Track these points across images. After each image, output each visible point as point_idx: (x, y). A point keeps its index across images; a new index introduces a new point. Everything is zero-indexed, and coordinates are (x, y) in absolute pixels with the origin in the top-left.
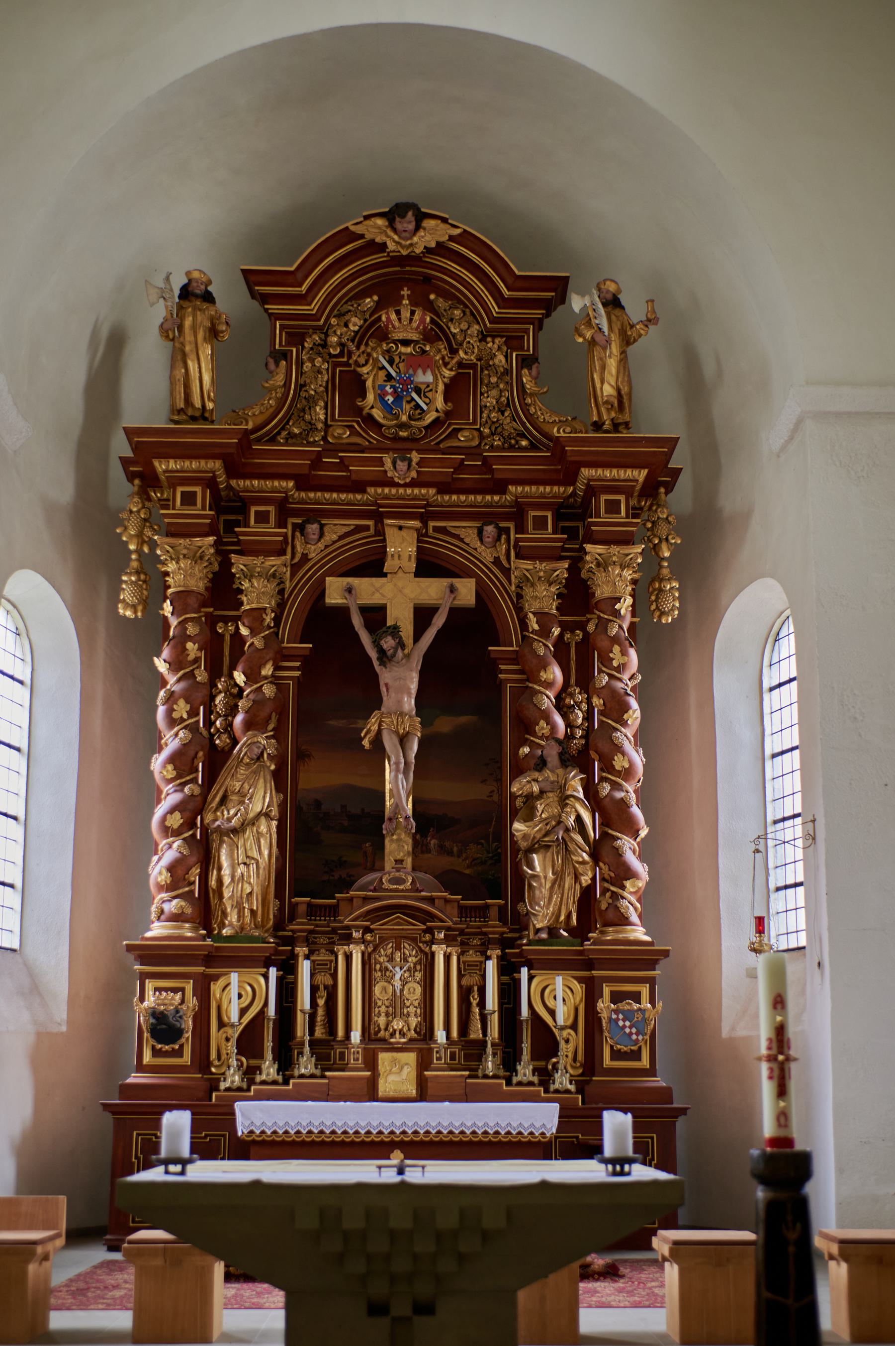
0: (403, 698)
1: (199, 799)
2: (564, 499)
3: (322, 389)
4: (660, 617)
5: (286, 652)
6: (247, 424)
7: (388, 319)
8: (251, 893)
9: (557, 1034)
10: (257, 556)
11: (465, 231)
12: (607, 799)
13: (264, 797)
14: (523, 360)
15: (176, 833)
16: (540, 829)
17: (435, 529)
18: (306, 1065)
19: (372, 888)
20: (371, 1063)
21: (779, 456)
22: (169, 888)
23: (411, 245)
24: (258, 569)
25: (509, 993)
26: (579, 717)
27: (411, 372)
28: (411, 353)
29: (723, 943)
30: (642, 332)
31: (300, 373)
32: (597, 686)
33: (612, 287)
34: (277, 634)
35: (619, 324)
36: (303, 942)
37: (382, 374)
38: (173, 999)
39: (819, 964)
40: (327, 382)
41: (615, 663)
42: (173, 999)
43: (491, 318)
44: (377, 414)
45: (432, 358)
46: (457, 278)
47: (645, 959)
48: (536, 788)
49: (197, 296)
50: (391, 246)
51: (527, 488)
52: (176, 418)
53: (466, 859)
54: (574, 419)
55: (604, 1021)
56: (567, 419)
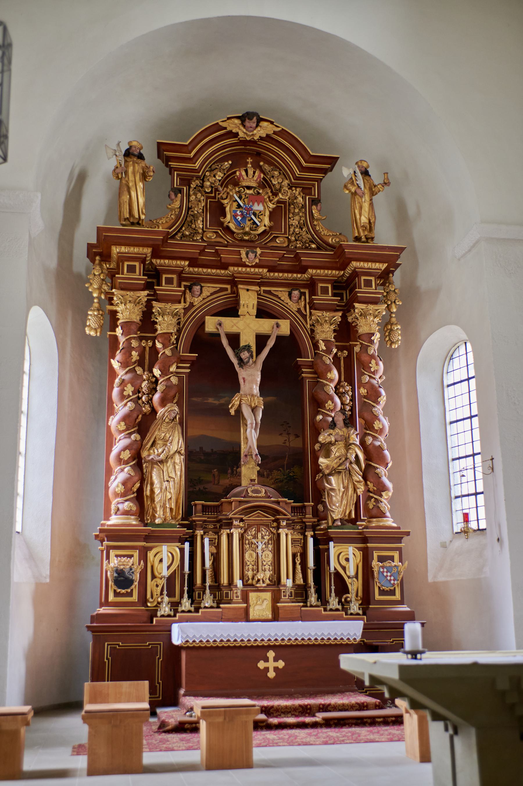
0: (253, 387)
1: (139, 442)
2: (338, 278)
3: (201, 211)
4: (391, 345)
6: (158, 228)
7: (241, 174)
8: (171, 498)
9: (347, 581)
10: (167, 303)
12: (371, 446)
13: (178, 442)
14: (313, 201)
15: (126, 463)
16: (337, 463)
17: (265, 291)
18: (208, 601)
19: (243, 495)
20: (245, 599)
21: (459, 260)
22: (123, 495)
23: (253, 135)
24: (168, 311)
25: (321, 557)
27: (251, 204)
28: (252, 194)
29: (427, 528)
30: (381, 189)
31: (189, 201)
32: (363, 382)
33: (365, 164)
34: (177, 347)
36: (200, 527)
37: (235, 204)
38: (129, 561)
39: (498, 539)
41: (372, 370)
42: (129, 561)
43: (295, 177)
44: (232, 226)
45: (263, 197)
47: (395, 537)
48: (333, 439)
49: (134, 155)
50: (241, 134)
51: (319, 271)
53: (272, 479)
54: (340, 234)
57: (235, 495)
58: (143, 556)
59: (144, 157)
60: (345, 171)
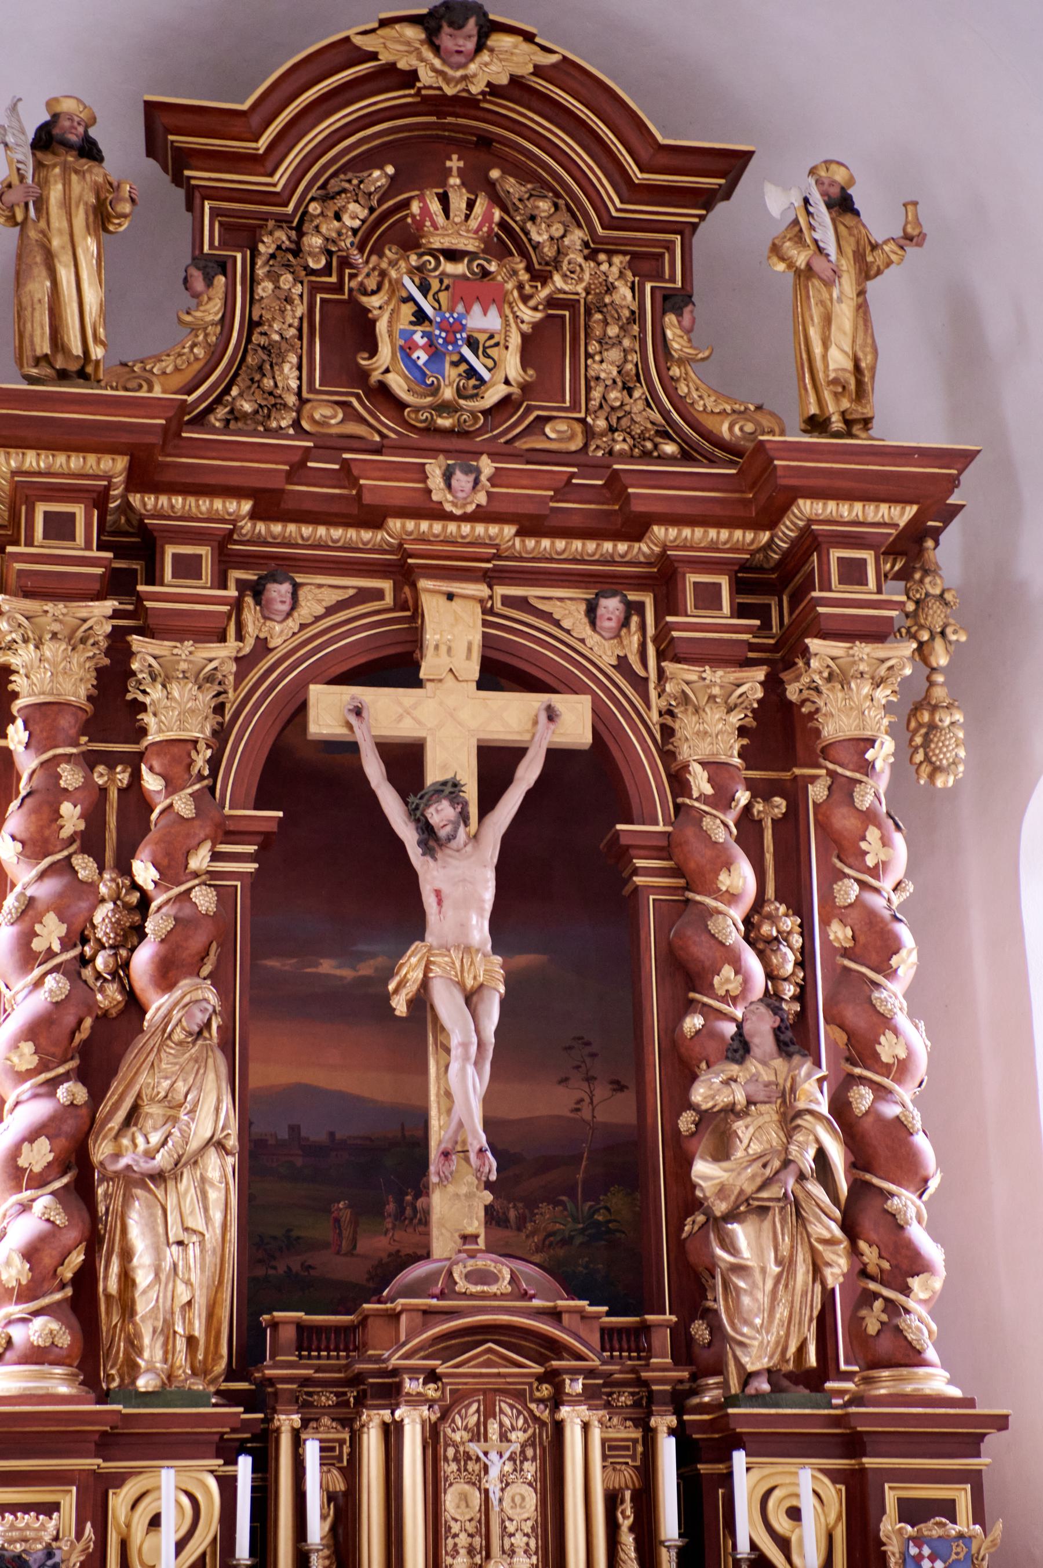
0: (469, 919)
1: (84, 1111)
2: (753, 553)
3: (293, 331)
4: (931, 777)
5: (231, 826)
6: (150, 390)
8: (189, 1303)
10: (182, 641)
11: (565, 58)
12: (870, 1119)
13: (217, 1110)
14: (666, 298)
15: (39, 1181)
16: (753, 1177)
17: (507, 601)
19: (437, 1290)
23: (465, 78)
24: (183, 666)
26: (787, 960)
27: (460, 308)
28: (464, 276)
30: (893, 257)
31: (252, 299)
33: (840, 175)
34: (212, 789)
35: (852, 240)
36: (289, 1403)
37: (407, 310)
38: (43, 1527)
40: (301, 319)
41: (870, 861)
44: (397, 384)
45: (501, 285)
46: (544, 143)
49: (68, 146)
50: (426, 77)
51: (687, 532)
52: (34, 371)
53: (533, 1233)
54: (759, 408)
55: (893, 1560)
56: (746, 409)
57: (411, 1291)
58: (95, 1510)
59: (99, 151)
60: (773, 197)
